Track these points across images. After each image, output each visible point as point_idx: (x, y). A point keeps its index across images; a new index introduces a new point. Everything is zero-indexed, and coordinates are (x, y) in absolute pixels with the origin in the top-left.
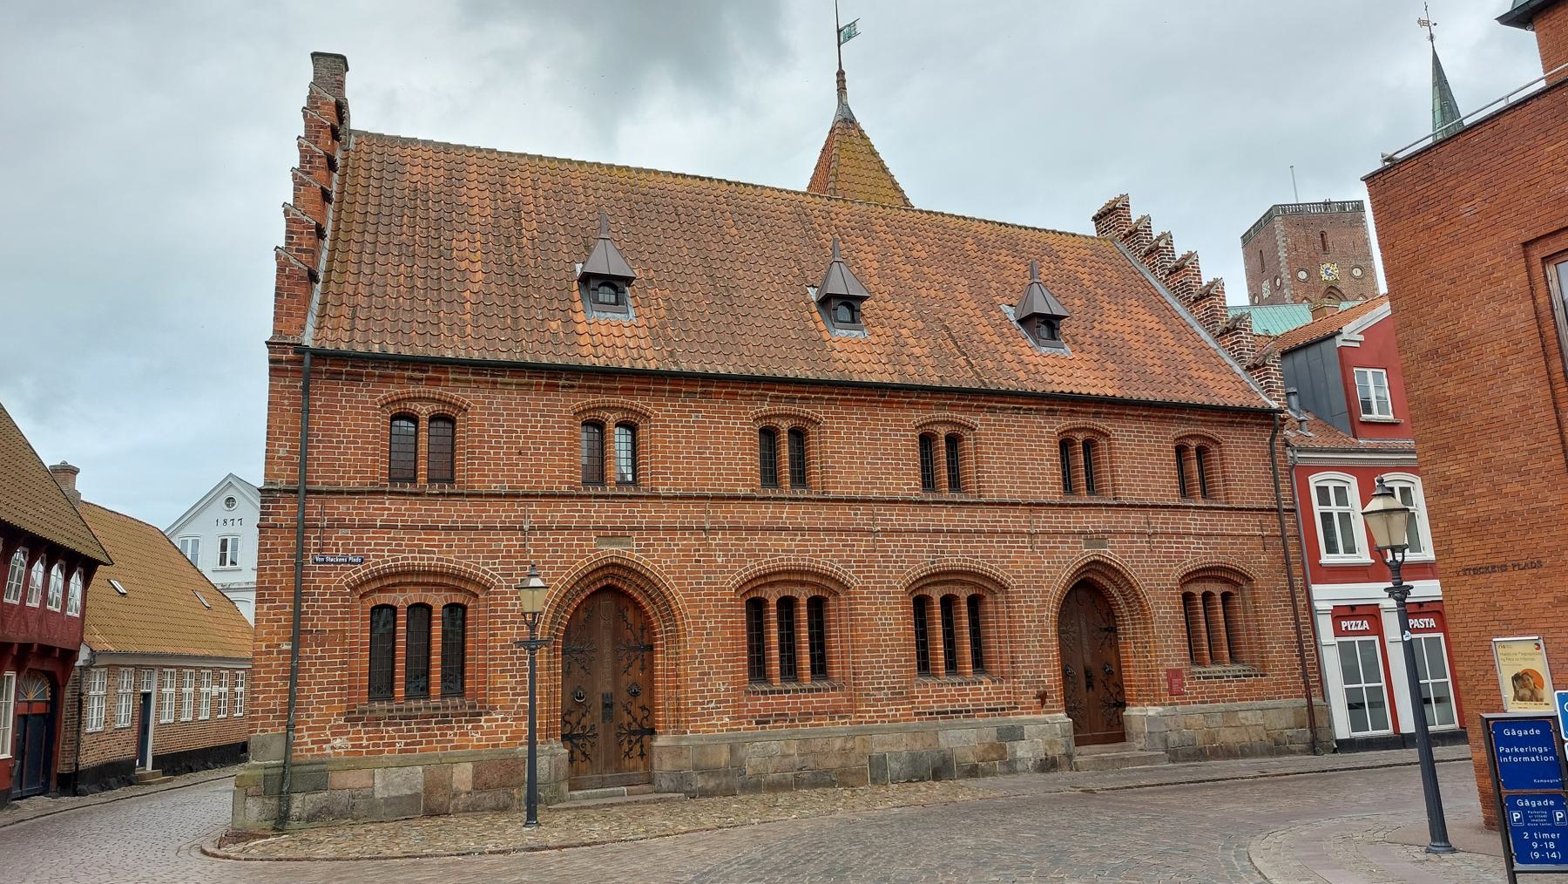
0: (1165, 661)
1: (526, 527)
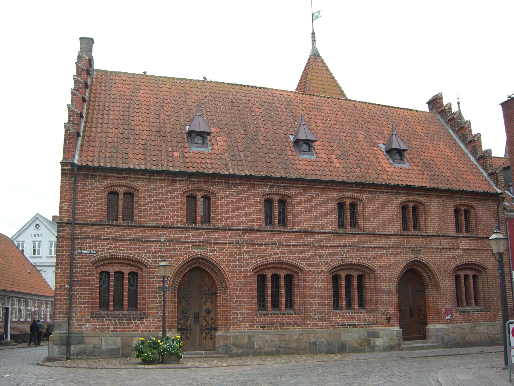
0: (445, 304)
1: (162, 240)
